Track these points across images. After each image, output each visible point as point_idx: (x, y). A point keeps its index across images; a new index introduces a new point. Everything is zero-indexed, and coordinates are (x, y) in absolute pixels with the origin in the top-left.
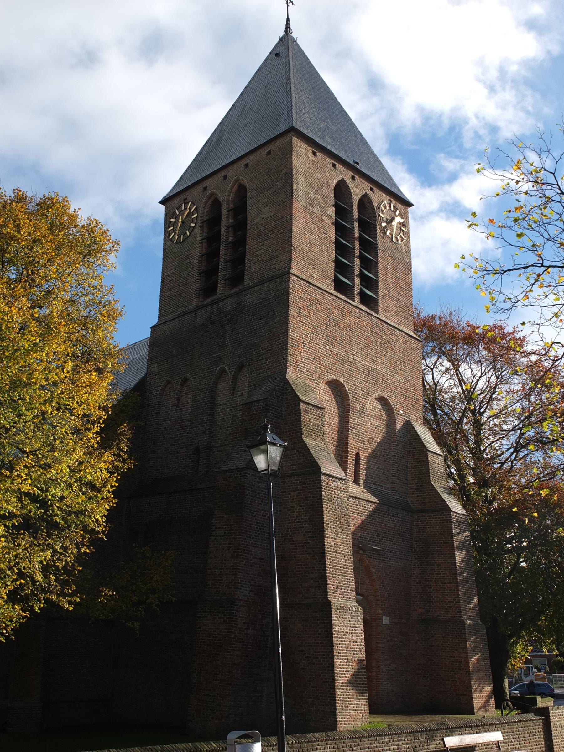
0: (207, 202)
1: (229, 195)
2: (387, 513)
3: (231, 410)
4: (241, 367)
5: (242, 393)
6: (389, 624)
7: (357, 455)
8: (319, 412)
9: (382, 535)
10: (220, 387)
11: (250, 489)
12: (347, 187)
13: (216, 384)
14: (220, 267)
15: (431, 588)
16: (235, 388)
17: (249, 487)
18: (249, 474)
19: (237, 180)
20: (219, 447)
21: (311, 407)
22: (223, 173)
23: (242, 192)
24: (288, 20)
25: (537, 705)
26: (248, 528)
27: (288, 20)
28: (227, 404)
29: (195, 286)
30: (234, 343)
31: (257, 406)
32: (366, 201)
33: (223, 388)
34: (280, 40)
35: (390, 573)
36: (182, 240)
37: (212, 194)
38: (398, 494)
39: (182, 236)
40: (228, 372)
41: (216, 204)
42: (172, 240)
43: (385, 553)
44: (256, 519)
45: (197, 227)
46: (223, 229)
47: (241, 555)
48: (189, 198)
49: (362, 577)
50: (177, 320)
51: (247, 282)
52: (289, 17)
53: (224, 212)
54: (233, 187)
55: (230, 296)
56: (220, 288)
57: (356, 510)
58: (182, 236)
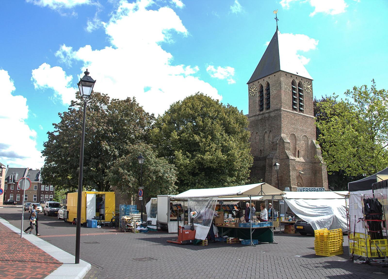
4: (271, 131)
7: (299, 151)
12: (295, 81)
13: (264, 135)
19: (267, 81)
23: (268, 85)
24: (277, 26)
25: (274, 235)
27: (277, 26)
29: (258, 108)
33: (266, 136)
37: (261, 84)
41: (262, 87)
42: (251, 95)
46: (264, 94)
48: (255, 84)
51: (271, 110)
53: (264, 90)
55: (267, 113)
56: (264, 110)
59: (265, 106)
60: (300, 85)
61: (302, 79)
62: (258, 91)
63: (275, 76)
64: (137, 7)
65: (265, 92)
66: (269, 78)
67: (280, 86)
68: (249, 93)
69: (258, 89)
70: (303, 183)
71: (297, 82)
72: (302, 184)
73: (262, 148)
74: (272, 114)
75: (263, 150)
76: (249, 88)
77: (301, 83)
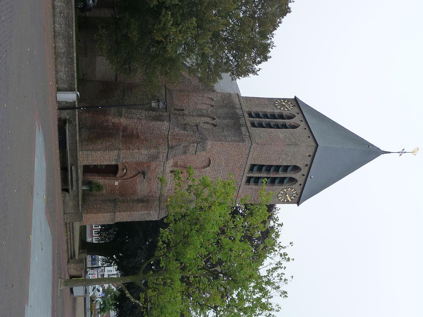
0: (292, 114)
1: (293, 123)
2: (158, 185)
3: (198, 122)
5: (205, 126)
6: (115, 184)
8: (194, 152)
9: (150, 182)
10: (208, 118)
11: (163, 124)
12: (298, 172)
14: (261, 119)
15: (129, 203)
16: (207, 124)
17: (163, 124)
18: (168, 124)
20: (184, 118)
21: (196, 149)
22: (303, 120)
24: (390, 153)
26: (148, 123)
27: (390, 153)
28: (201, 121)
30: (58, 20)
31: (196, 128)
32: (294, 182)
33: (208, 120)
34: (378, 148)
35: (135, 186)
36: (276, 105)
38: (167, 192)
39: (278, 105)
40: (214, 121)
41: (290, 117)
43: (142, 184)
44: (152, 126)
45: (281, 111)
47: (138, 120)
48: (295, 107)
49: (133, 173)
50: (239, 103)
52: (391, 153)
54: (297, 124)
57: (159, 170)
58: (278, 105)
59: (257, 120)
60: (292, 180)
61: (300, 184)
62: (283, 112)
63: (309, 137)
64: (292, 245)
65: (280, 121)
66: (306, 129)
67: (291, 143)
68: (280, 99)
69: (286, 112)
70: (126, 179)
71: (297, 176)
72: (125, 177)
73: (186, 112)
74: (243, 129)
75: (184, 115)
76: (289, 100)
77: (294, 184)
